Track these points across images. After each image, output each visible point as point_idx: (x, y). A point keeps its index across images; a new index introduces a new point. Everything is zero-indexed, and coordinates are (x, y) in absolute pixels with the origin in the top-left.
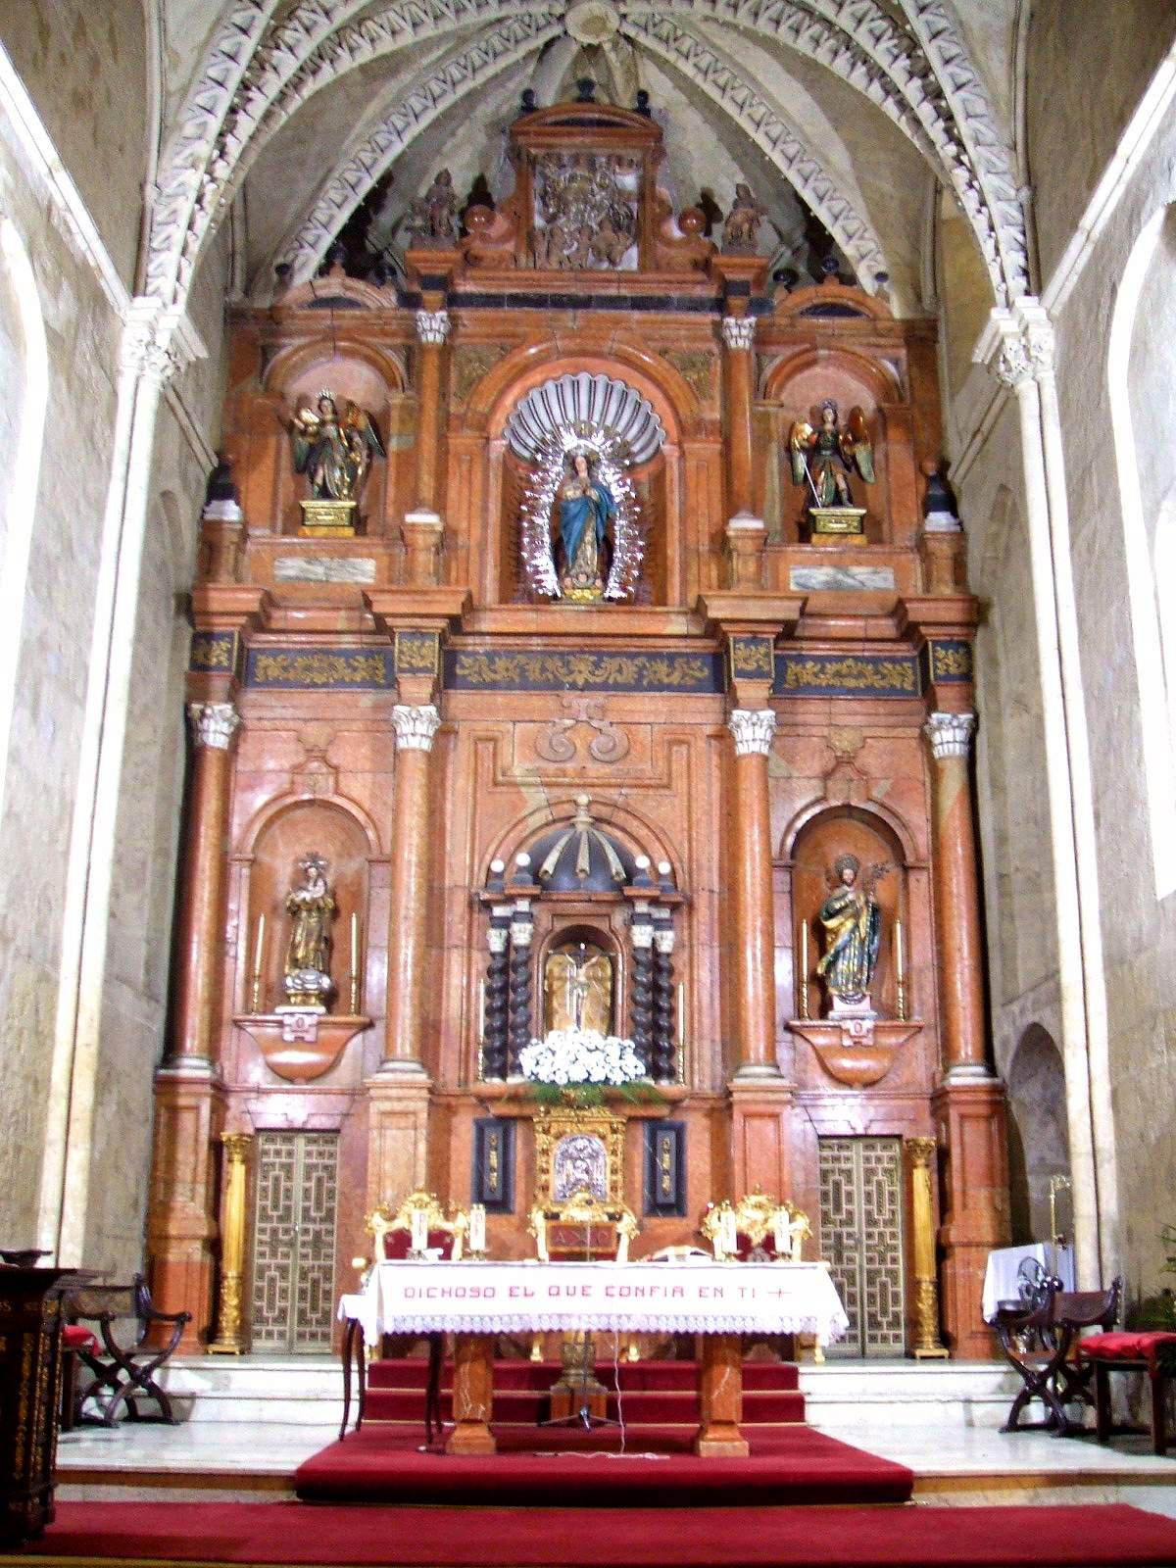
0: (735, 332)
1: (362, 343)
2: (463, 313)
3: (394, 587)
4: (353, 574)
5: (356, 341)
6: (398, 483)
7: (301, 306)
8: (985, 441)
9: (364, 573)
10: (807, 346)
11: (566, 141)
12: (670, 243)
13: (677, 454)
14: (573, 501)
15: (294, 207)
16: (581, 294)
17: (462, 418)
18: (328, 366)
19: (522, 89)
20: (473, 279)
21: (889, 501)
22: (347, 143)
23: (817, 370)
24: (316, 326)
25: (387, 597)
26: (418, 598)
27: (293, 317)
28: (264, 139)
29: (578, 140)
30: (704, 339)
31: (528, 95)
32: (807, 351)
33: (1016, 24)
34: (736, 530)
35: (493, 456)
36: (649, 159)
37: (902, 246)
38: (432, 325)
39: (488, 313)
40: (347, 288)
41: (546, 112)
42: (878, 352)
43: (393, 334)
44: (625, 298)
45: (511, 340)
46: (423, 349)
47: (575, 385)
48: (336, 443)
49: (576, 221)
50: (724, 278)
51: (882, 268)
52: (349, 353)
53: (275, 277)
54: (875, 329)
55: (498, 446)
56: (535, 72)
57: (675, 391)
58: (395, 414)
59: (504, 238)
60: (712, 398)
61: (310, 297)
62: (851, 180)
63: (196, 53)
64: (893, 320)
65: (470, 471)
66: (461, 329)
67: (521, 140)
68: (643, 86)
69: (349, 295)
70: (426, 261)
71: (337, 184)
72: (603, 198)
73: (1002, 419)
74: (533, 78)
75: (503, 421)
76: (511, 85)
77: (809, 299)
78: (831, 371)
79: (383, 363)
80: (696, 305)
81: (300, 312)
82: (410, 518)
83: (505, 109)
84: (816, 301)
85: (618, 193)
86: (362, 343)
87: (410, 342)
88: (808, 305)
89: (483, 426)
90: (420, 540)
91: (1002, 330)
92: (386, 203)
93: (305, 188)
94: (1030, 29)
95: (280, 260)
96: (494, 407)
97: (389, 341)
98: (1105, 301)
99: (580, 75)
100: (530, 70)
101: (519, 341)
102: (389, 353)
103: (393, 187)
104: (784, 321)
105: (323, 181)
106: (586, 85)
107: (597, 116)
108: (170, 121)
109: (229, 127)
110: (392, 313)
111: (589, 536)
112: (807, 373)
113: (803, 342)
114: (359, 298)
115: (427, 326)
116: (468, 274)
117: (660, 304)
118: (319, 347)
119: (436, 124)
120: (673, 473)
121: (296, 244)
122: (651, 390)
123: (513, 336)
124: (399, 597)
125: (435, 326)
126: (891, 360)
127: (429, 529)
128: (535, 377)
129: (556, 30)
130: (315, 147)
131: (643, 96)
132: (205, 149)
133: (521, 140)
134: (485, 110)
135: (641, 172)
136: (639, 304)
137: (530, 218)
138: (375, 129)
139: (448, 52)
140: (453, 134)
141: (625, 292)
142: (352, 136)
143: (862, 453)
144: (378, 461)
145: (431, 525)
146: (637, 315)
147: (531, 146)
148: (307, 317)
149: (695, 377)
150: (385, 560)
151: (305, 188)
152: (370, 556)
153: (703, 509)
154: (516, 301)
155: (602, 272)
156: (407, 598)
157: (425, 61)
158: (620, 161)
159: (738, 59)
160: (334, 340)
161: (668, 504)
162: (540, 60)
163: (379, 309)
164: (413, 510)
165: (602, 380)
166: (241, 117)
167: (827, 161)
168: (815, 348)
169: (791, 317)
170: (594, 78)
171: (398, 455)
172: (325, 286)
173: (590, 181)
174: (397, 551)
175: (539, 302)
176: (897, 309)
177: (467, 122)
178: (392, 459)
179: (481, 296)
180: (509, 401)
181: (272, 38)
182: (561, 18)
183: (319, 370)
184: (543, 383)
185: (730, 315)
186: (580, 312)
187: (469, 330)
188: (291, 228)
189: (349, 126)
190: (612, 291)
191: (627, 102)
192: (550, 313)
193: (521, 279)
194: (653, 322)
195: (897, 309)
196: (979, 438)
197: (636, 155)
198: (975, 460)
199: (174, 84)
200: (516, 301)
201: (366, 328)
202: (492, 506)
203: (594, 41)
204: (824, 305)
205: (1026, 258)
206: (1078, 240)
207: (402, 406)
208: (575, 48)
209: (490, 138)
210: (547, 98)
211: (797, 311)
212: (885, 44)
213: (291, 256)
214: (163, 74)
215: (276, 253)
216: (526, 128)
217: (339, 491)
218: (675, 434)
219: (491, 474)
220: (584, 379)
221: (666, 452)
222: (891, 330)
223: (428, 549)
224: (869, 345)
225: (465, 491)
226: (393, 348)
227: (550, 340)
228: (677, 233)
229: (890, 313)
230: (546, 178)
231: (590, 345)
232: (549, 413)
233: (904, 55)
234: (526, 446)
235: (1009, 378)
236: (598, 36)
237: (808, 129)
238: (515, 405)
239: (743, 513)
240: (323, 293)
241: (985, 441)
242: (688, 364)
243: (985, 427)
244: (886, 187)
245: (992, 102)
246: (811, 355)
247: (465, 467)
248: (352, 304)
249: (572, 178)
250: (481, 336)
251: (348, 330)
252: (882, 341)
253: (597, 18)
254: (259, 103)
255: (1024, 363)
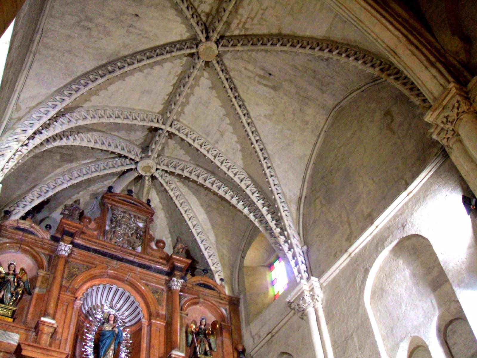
0: (176, 283)
1: (33, 249)
2: (76, 250)
3: (35, 345)
4: (8, 339)
5: (31, 248)
6: (35, 306)
7: (11, 227)
8: (272, 337)
9: (13, 340)
10: (196, 296)
11: (121, 206)
12: (153, 249)
13: (147, 324)
14: (107, 331)
15: (19, 193)
16: (120, 256)
17: (67, 288)
18: (15, 254)
19: (110, 185)
20: (82, 238)
21: (233, 354)
22: (45, 179)
23: (198, 306)
24: (14, 236)
25: (29, 348)
26: (44, 352)
27: (7, 231)
28: (37, 151)
29: (125, 207)
30: (161, 285)
31: (110, 188)
32: (196, 298)
33: (300, 198)
34: (175, 355)
35: (75, 307)
36: (148, 220)
37: (228, 272)
38: (65, 249)
39: (85, 253)
40: (32, 227)
41: (116, 195)
42: (220, 305)
43: (46, 249)
44: (135, 262)
45: (91, 265)
46: (59, 257)
47: (110, 289)
48: (12, 283)
49: (123, 230)
50: (174, 264)
51: (222, 277)
52: (25, 251)
53: (3, 214)
54: (220, 296)
55: (78, 303)
56: (115, 181)
57: (150, 300)
58: (40, 279)
59: (95, 230)
60: (163, 306)
61: (16, 226)
62: (215, 246)
63: (28, 109)
64: (226, 295)
65: (67, 310)
66: (73, 255)
67: (106, 200)
68: (150, 198)
69: (32, 229)
70: (69, 225)
71: (38, 190)
72: (134, 226)
73: (285, 327)
74: (114, 182)
75: (81, 294)
76: (105, 183)
77: (199, 281)
78: (202, 308)
79: (39, 259)
80: (160, 272)
81: (10, 230)
82: (43, 319)
83: (100, 190)
84: (201, 282)
85: (138, 227)
86: (33, 249)
87: (51, 254)
88: (198, 282)
89: (74, 292)
90: (46, 329)
91: (303, 288)
92: (43, 210)
93: (25, 187)
94: (305, 201)
95: (7, 209)
96: (81, 286)
97: (43, 251)
98: (360, 276)
99: (129, 188)
100: (114, 180)
101: (94, 266)
102: (42, 255)
103: (48, 205)
104: (190, 286)
105: (34, 187)
106: (130, 192)
107: (133, 202)
108: (10, 126)
109: (32, 138)
110: (47, 241)
111: (112, 347)
112: (194, 307)
113: (194, 294)
114: (35, 232)
115: (63, 248)
116: (81, 236)
117: (148, 268)
118: (14, 245)
119: (73, 186)
120: (145, 330)
121: (16, 205)
122: (139, 299)
123: (93, 264)
124: (35, 350)
125: (66, 249)
126: (224, 308)
127: (51, 326)
128: (96, 282)
129: (133, 167)
130: (33, 176)
131: (149, 201)
132: (23, 138)
133: (106, 200)
134: (94, 188)
135: (145, 224)
136: (140, 266)
137: (105, 226)
138: (58, 177)
139: (92, 162)
140: (78, 193)
141: (136, 260)
142: (49, 177)
143: (212, 340)
144: (26, 297)
145: (53, 324)
146: (139, 269)
147: (109, 203)
148: (12, 233)
149: (157, 297)
150: (24, 336)
151: (25, 187)
152: (18, 333)
153: (156, 347)
154: (96, 251)
155: (129, 250)
156: (39, 351)
157: (83, 162)
158: (139, 218)
159: (186, 197)
160: (21, 244)
161: (142, 343)
162: (119, 177)
163: (43, 238)
164: (44, 316)
165: (121, 290)
166: (37, 136)
167: (208, 237)
168: (199, 298)
169: (193, 285)
170: (133, 190)
171: (38, 295)
172: (23, 224)
173: (130, 220)
174: (31, 333)
175: (104, 254)
176: (227, 291)
177: (85, 190)
178: (35, 296)
179: (82, 245)
180: (85, 287)
181: (55, 119)
182: (137, 163)
183: (8, 255)
184: (99, 285)
185: (175, 277)
186: (119, 262)
187: (76, 257)
188: (14, 200)
189: (48, 173)
190: (131, 258)
191: (144, 200)
192: (107, 259)
193: (99, 243)
194: (145, 274)
195: (227, 291)
196: (270, 336)
197: (144, 218)
198: (265, 344)
199: (16, 115)
200: (96, 251)
201: (35, 244)
202: (71, 326)
203: (144, 174)
204: (203, 284)
205: (307, 268)
206: (346, 256)
207: (43, 276)
208: (136, 175)
209: (91, 199)
210: (118, 190)
211: (194, 283)
212: (255, 195)
213: (12, 209)
214: (12, 112)
215: (6, 206)
216: (110, 197)
217: (9, 303)
218: (146, 316)
219: (73, 314)
220: (114, 287)
221: (143, 322)
222: (225, 298)
223: (48, 334)
224: (217, 302)
225: (63, 317)
226: (44, 254)
227: (106, 269)
228: (154, 247)
229: (225, 292)
230: (113, 214)
231: (120, 275)
232: (96, 298)
233: (262, 200)
234: (85, 309)
235: (304, 306)
236: (146, 173)
237: (204, 226)
238: (87, 289)
239: (177, 349)
240: (22, 226)
241: (272, 337)
242: (155, 291)
243: (274, 332)
244: (225, 252)
245: (293, 219)
246: (197, 300)
247: (65, 307)
248: (31, 233)
249: (123, 217)
250: (80, 260)
251: (27, 242)
252: (221, 301)
253: (149, 166)
254: (46, 134)
255: (311, 301)
